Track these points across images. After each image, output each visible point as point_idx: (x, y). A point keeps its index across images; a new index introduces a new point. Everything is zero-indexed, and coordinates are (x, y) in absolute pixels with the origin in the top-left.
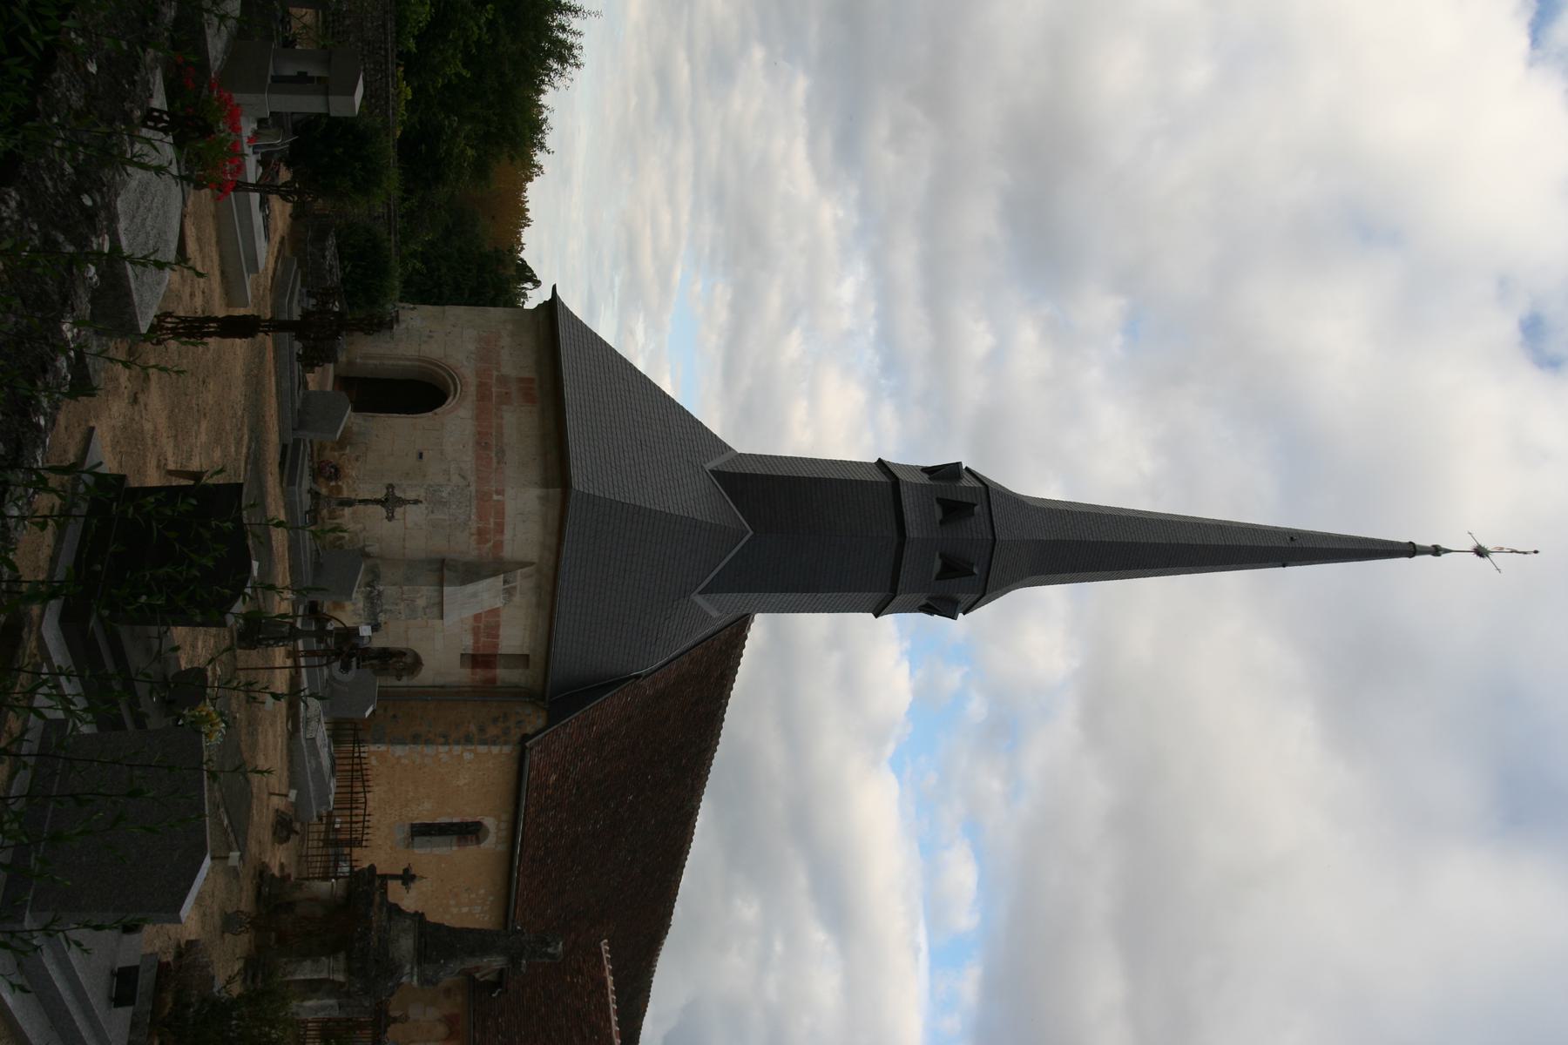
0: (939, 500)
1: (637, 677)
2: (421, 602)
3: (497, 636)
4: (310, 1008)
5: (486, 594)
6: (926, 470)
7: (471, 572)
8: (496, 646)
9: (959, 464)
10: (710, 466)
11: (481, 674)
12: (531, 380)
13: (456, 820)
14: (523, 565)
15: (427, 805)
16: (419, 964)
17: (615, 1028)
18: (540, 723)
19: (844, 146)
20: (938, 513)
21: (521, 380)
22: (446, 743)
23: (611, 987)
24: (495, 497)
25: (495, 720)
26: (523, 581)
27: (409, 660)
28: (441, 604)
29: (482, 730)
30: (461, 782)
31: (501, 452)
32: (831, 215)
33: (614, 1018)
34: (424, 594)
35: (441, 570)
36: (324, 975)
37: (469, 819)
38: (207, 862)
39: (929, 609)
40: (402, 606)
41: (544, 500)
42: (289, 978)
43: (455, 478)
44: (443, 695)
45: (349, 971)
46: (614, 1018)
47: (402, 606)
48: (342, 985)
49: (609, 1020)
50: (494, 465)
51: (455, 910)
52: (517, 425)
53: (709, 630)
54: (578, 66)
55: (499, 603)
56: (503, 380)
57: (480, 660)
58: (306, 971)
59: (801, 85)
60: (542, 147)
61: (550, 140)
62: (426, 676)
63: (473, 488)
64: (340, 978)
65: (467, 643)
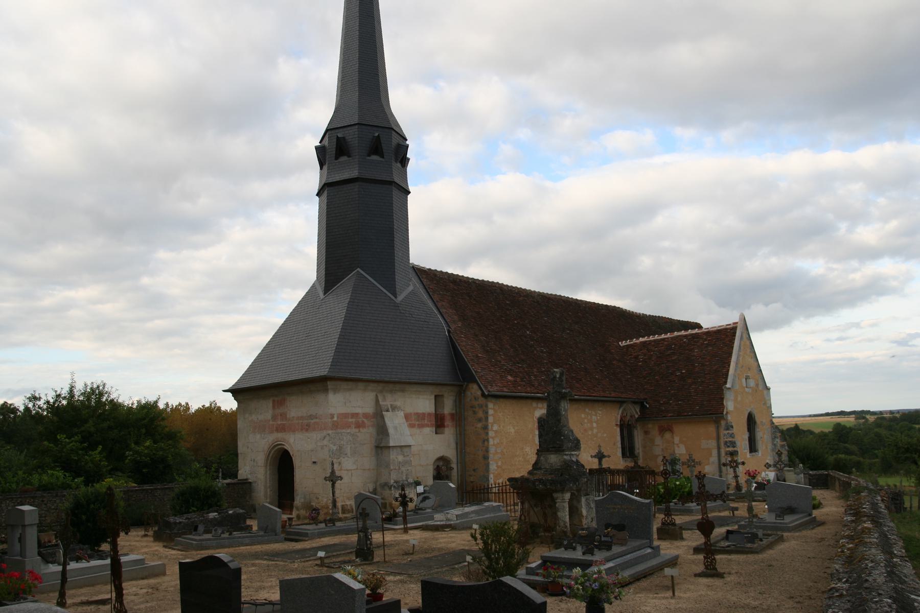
0: (336, 158)
1: (449, 332)
2: (401, 458)
3: (424, 414)
4: (588, 512)
5: (395, 422)
6: (321, 169)
7: (382, 431)
8: (429, 414)
9: (317, 148)
10: (322, 296)
11: (448, 422)
12: (274, 401)
13: (537, 432)
14: (377, 401)
15: (528, 449)
16: (563, 451)
17: (669, 335)
18: (475, 386)
19: (198, 227)
20: (344, 159)
21: (274, 407)
22: (488, 440)
23: (646, 339)
24: (335, 419)
25: (475, 413)
26: (387, 401)
27: (441, 463)
28: (401, 447)
29: (480, 420)
30: (512, 430)
31: (311, 417)
32: (238, 232)
33: (663, 336)
34: (395, 457)
35: (381, 448)
36: (566, 505)
37: (536, 425)
38: (340, 576)
39: (404, 161)
40: (403, 469)
41: (335, 391)
42: (568, 525)
43: (325, 442)
44: (461, 444)
45: (563, 491)
46: (663, 336)
47: (403, 469)
48: (572, 494)
49: (663, 339)
50: (317, 420)
51: (595, 431)
52: (297, 408)
53: (422, 291)
54: (104, 385)
55: (401, 414)
56: (274, 418)
57: (439, 423)
58: (564, 515)
59: (162, 255)
60: (156, 402)
61: (152, 399)
62: (451, 454)
63: (330, 432)
64: (567, 496)
65: (428, 431)
